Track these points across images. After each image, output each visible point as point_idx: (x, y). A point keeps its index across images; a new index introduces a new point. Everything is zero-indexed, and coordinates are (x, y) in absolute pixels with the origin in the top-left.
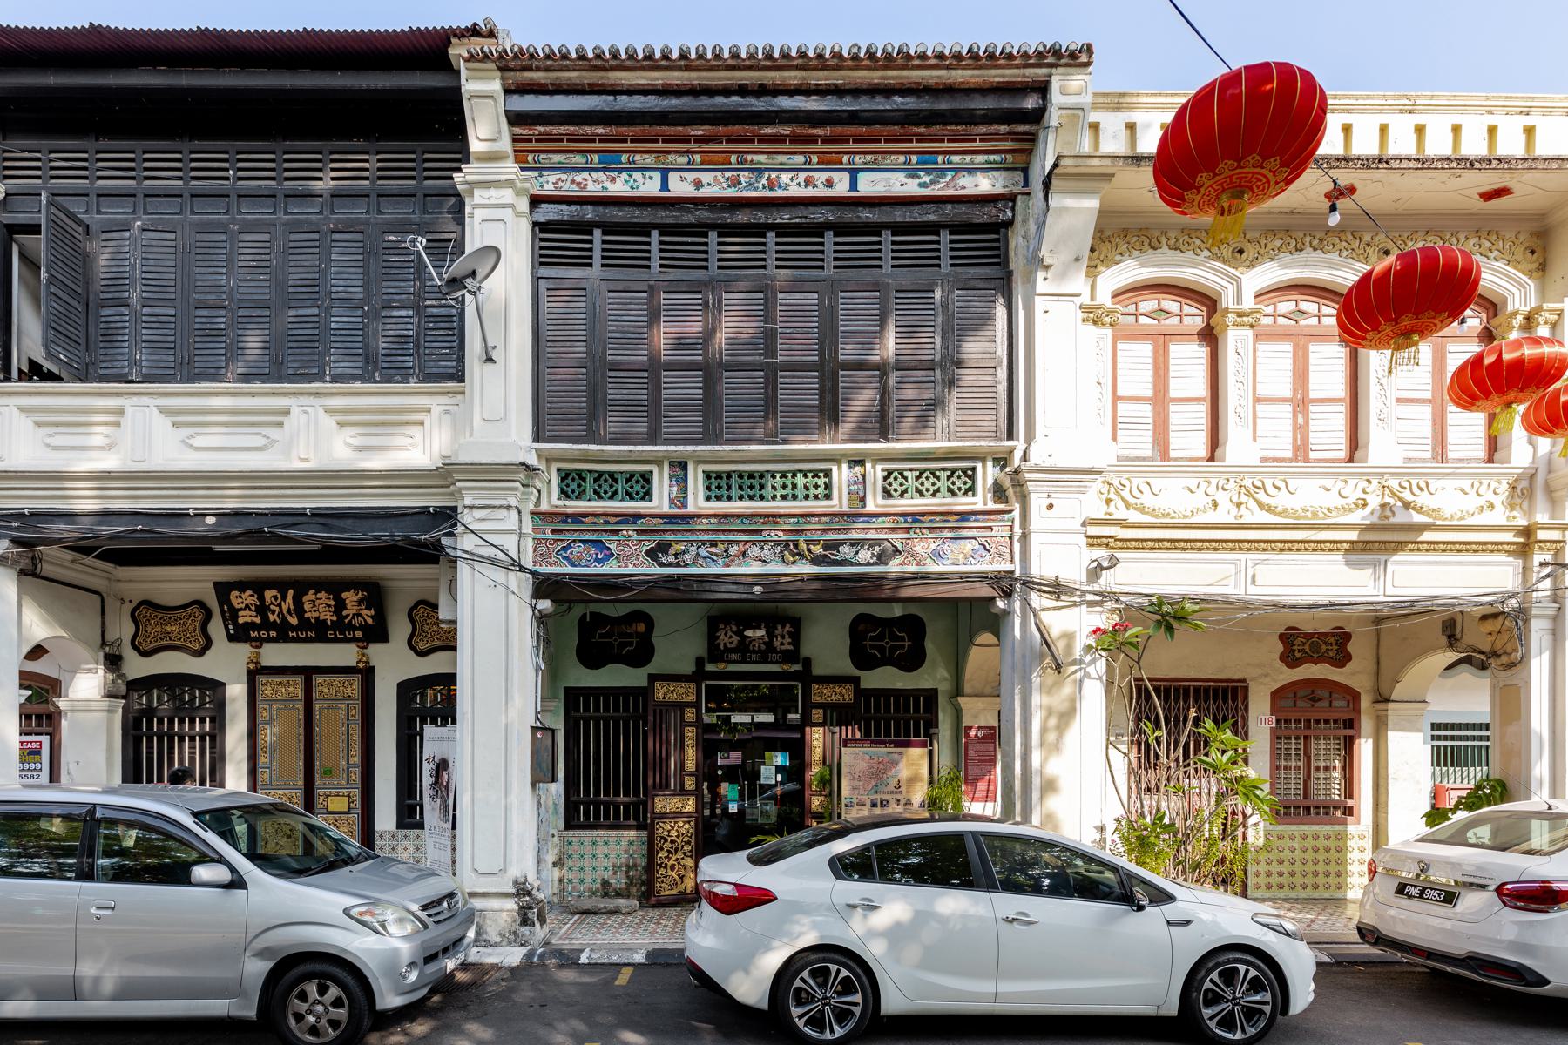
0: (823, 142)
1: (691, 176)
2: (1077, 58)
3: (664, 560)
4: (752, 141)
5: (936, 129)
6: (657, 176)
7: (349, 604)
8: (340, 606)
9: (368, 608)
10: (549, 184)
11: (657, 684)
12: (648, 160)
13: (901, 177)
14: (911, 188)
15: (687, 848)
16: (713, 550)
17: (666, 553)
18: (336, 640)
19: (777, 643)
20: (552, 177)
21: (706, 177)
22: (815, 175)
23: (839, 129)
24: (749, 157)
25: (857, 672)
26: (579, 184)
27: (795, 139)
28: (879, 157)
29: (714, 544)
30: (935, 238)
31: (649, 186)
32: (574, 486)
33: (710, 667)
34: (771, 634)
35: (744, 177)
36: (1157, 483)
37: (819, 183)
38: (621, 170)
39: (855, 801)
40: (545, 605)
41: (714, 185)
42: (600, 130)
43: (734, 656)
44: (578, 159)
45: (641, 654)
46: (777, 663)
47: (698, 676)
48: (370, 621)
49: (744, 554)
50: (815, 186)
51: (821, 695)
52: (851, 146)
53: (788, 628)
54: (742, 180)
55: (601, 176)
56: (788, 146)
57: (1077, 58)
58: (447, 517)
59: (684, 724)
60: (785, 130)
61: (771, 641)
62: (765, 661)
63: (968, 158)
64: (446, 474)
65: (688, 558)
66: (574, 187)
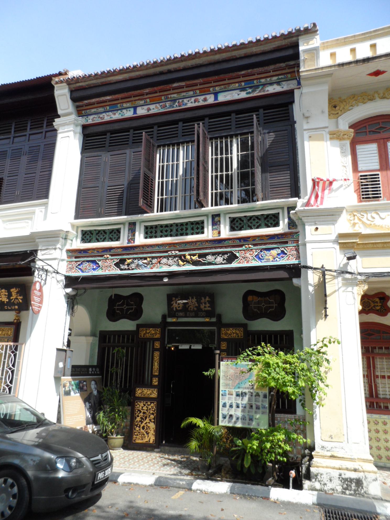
0: (200, 85)
1: (146, 107)
2: (310, 31)
3: (122, 267)
4: (170, 90)
5: (222, 76)
6: (132, 110)
7: (13, 294)
8: (10, 295)
9: (20, 296)
10: (90, 120)
11: (141, 329)
12: (128, 105)
13: (238, 91)
14: (243, 95)
15: (152, 416)
16: (145, 261)
17: (123, 264)
18: (8, 310)
19: (202, 307)
20: (91, 117)
21: (152, 107)
22: (199, 97)
23: (206, 79)
24: (169, 96)
25: (246, 321)
26: (101, 118)
27: (188, 86)
28: (227, 86)
29: (145, 258)
30: (177, 126)
31: (129, 114)
32: (88, 237)
33: (169, 320)
34: (199, 302)
35: (168, 104)
36: (383, 215)
37: (200, 100)
38: (118, 110)
39: (227, 392)
40: (69, 290)
41: (155, 109)
42: (108, 98)
43: (181, 314)
44: (101, 110)
45: (136, 314)
46: (203, 317)
47: (164, 324)
48: (21, 301)
49: (159, 262)
50: (199, 102)
51: (226, 334)
52: (213, 84)
53: (207, 299)
54: (167, 105)
55: (110, 113)
56: (185, 89)
57: (310, 31)
58: (34, 253)
59: (154, 350)
60: (183, 84)
61: (199, 306)
62: (196, 316)
63: (268, 79)
64: (33, 237)
65: (133, 266)
66: (99, 119)
